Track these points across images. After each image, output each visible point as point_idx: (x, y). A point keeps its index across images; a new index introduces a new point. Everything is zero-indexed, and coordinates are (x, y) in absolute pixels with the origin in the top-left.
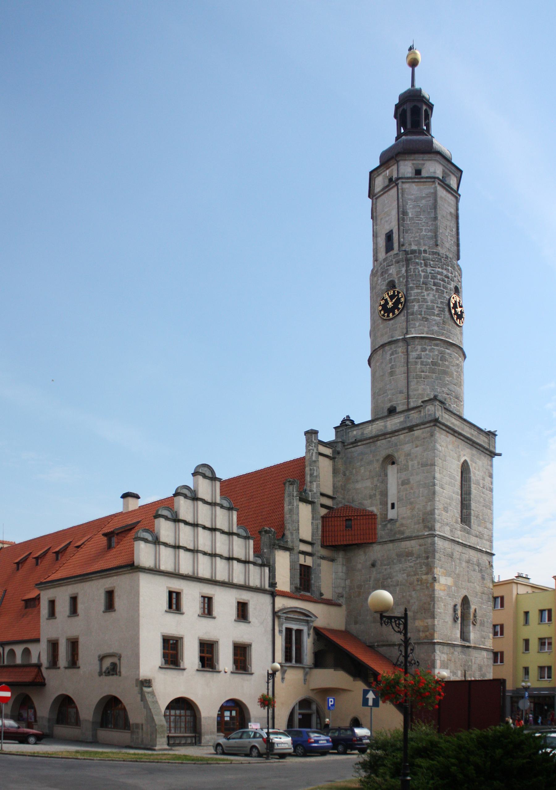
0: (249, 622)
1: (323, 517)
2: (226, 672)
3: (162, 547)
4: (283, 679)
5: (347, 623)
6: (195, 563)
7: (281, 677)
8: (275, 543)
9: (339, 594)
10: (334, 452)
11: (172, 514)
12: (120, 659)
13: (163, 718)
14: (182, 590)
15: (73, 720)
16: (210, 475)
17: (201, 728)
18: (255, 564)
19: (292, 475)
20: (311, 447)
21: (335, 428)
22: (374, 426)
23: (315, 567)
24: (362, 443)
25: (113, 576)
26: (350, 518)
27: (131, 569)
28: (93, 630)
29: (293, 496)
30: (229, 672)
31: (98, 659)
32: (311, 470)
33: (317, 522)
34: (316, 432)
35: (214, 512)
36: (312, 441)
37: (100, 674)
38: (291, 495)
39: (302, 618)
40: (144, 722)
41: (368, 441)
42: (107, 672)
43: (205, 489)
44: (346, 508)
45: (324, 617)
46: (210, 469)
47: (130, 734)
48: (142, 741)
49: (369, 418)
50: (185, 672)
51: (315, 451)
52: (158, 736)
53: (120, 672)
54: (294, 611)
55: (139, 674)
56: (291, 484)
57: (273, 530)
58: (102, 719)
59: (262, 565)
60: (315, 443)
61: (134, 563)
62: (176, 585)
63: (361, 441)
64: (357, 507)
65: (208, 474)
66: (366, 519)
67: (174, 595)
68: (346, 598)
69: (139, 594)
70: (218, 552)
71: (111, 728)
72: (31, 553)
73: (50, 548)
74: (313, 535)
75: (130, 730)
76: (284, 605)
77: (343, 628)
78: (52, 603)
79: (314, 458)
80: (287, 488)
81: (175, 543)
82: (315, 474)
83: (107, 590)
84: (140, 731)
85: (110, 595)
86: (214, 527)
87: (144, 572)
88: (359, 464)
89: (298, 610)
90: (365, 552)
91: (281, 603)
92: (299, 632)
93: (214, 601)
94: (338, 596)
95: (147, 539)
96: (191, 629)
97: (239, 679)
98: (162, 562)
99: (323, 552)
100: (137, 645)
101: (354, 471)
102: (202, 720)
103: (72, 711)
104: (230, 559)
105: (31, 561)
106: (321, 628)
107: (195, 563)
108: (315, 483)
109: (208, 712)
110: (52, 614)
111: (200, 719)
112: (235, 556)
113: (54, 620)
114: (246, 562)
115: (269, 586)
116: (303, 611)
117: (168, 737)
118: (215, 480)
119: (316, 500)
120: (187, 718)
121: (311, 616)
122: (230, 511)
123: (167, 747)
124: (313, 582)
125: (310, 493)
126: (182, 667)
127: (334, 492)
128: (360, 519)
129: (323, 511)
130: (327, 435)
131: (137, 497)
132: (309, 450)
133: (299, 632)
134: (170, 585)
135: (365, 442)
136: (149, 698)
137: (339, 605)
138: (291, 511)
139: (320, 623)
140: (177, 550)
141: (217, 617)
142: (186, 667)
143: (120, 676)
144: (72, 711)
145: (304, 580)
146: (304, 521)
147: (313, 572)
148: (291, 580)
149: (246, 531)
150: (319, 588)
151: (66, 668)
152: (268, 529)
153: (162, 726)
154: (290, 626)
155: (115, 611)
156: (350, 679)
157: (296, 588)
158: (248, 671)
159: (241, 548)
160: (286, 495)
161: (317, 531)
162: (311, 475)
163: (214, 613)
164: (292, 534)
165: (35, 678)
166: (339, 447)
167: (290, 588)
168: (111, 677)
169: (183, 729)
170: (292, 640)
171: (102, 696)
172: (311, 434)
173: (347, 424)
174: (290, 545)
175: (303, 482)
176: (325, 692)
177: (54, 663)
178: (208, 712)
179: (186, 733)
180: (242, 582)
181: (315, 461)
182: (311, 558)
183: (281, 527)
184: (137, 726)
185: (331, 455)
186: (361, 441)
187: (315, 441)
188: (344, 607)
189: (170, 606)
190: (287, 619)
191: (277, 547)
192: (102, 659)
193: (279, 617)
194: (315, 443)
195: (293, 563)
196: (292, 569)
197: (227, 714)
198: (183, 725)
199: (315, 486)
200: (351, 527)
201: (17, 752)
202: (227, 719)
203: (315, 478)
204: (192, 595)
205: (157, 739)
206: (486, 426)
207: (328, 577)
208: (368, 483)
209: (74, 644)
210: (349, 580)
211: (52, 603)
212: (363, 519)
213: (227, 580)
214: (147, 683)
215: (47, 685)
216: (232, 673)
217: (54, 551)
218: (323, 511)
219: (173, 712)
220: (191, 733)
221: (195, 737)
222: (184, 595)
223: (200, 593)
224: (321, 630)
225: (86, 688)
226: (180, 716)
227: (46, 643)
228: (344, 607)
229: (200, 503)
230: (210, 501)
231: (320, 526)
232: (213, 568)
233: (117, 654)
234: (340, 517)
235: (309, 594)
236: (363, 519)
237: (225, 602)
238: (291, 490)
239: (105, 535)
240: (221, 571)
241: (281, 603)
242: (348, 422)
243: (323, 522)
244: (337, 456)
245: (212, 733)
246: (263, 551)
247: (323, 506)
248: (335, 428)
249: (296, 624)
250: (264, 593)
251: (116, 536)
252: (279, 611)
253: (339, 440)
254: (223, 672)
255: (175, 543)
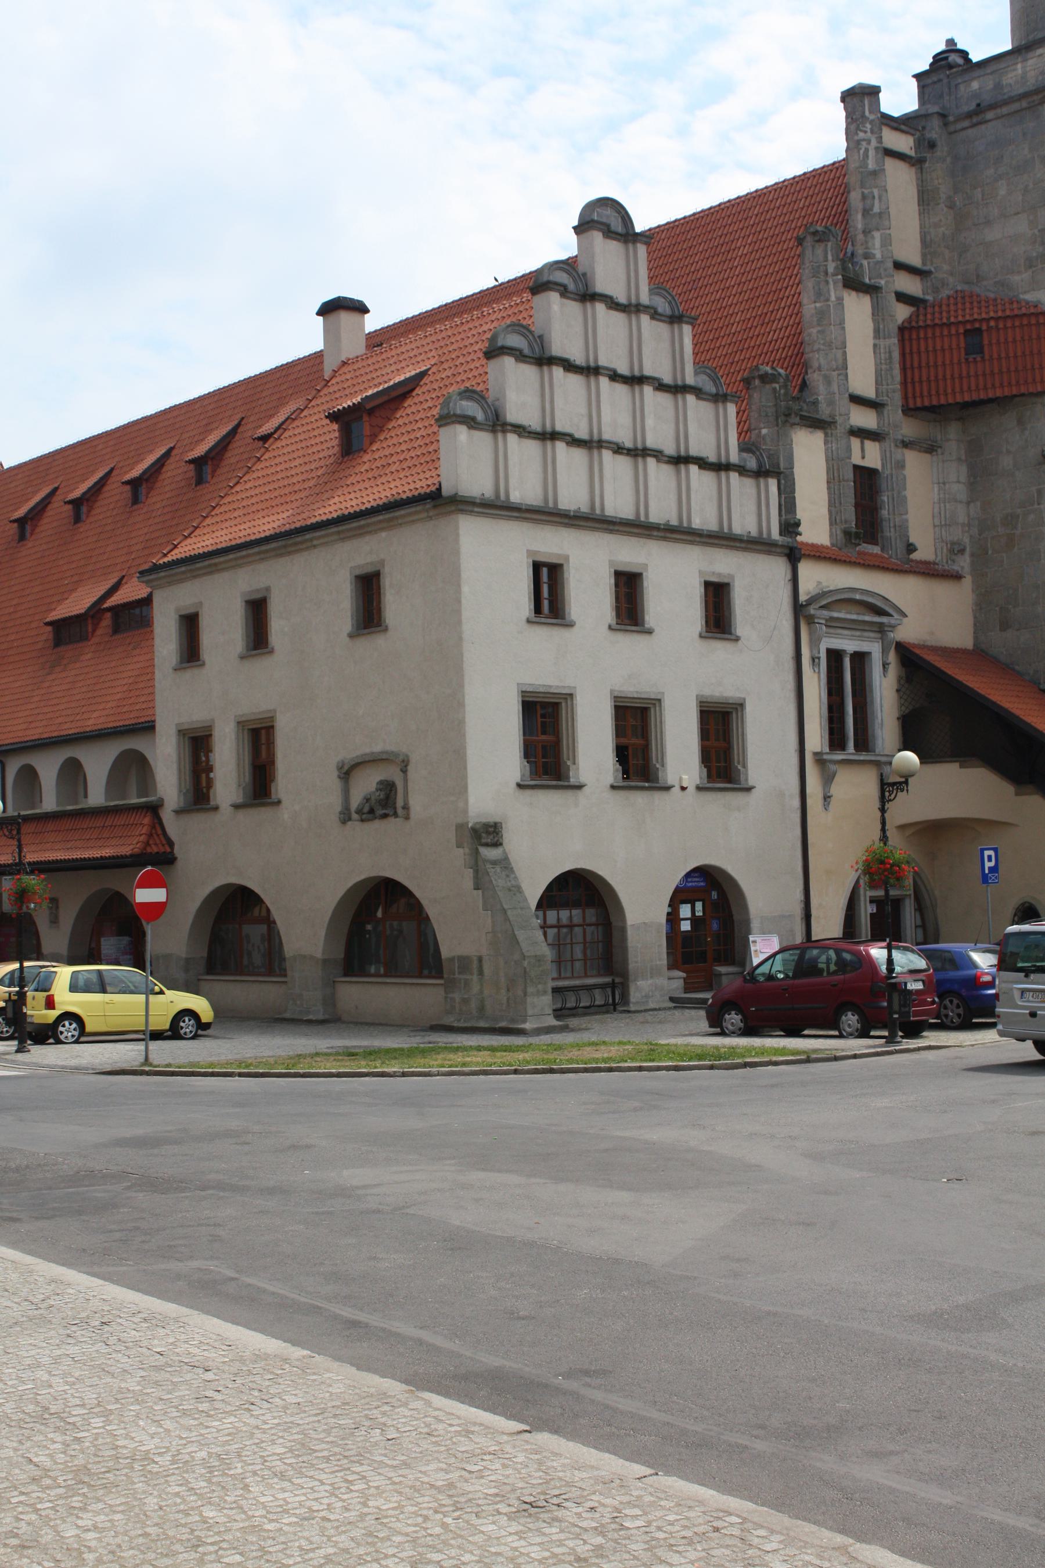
0: (737, 639)
1: (902, 329)
2: (683, 789)
3: (512, 438)
4: (827, 798)
5: (979, 627)
6: (594, 477)
7: (821, 796)
8: (788, 408)
9: (953, 543)
10: (918, 144)
11: (530, 345)
12: (404, 771)
13: (539, 934)
14: (567, 558)
15: (258, 959)
16: (620, 229)
17: (625, 961)
18: (742, 470)
19: (805, 216)
20: (861, 135)
21: (918, 77)
22: (1030, 62)
23: (888, 472)
24: (998, 111)
25: (376, 531)
26: (977, 325)
27: (435, 507)
28: (319, 692)
29: (826, 273)
30: (691, 789)
31: (336, 773)
32: (864, 197)
33: (888, 342)
34: (873, 92)
35: (634, 328)
36: (863, 116)
37: (345, 817)
38: (818, 272)
39: (867, 618)
40: (484, 952)
41: (1016, 106)
42: (366, 809)
43: (612, 270)
44: (961, 298)
45: (933, 614)
46: (619, 213)
47: (441, 991)
48: (482, 1009)
49: (1008, 47)
50: (581, 795)
51: (874, 143)
52: (530, 990)
53: (406, 807)
54: (848, 600)
55: (465, 811)
56: (819, 241)
57: (782, 371)
58: (211, 952)
59: (760, 473)
60: (871, 122)
61: (439, 489)
62: (553, 542)
63: (992, 107)
64: (992, 296)
65: (617, 226)
66: (1022, 326)
67: (545, 570)
68: (972, 555)
69: (459, 575)
70: (650, 443)
71: (377, 975)
72: (56, 490)
73: (112, 470)
74: (878, 383)
75: (441, 977)
76: (819, 583)
77: (968, 643)
78: (190, 624)
79: (871, 165)
80: (808, 253)
81: (544, 425)
82: (876, 209)
83: (358, 572)
84: (475, 977)
85: (369, 587)
86: (637, 373)
87: (471, 513)
88: (990, 172)
89: (858, 597)
90: (1020, 422)
91: (814, 577)
92: (860, 659)
93: (645, 584)
94: (951, 551)
95: (473, 419)
96: (591, 667)
97: (720, 804)
98: (513, 482)
99: (908, 429)
100: (459, 726)
101: (978, 193)
102: (630, 932)
103: (255, 932)
104: (680, 460)
105: (59, 510)
106: (915, 646)
107: (594, 477)
108: (877, 235)
109: (645, 909)
110: (191, 652)
111: (623, 930)
112: (694, 452)
113: (196, 671)
114: (720, 467)
115: (781, 534)
116: (870, 600)
117: (556, 990)
118: (634, 242)
119: (883, 282)
120: (589, 930)
121: (891, 611)
122: (676, 326)
123: (552, 1022)
124: (884, 513)
125: (865, 263)
126: (573, 781)
127: (924, 256)
128: (1005, 328)
129: (902, 312)
130: (900, 99)
131: (361, 309)
132: (858, 142)
133: (860, 659)
134: (535, 547)
135: (1005, 110)
136: (499, 881)
137: (957, 577)
138: (822, 315)
139: (908, 631)
140: (549, 444)
141: (657, 630)
142: (583, 778)
143: (407, 818)
144: (255, 932)
145: (866, 508)
146: (858, 346)
147: (884, 486)
148: (830, 512)
149: (715, 380)
150: (903, 529)
151: (237, 807)
152: (768, 369)
153: (539, 959)
154: (837, 643)
155: (386, 629)
156: (1009, 789)
157: (847, 533)
158: (738, 782)
159: (707, 428)
160: (806, 272)
161: (891, 369)
162: (866, 212)
163: (647, 618)
164: (828, 381)
165: (147, 844)
166: (934, 130)
167: (831, 536)
168: (377, 824)
169: (578, 965)
170: (845, 677)
171: (350, 884)
172: (860, 99)
173: (948, 67)
174: (824, 411)
175: (846, 237)
176: (933, 832)
177: (199, 795)
178: (645, 909)
179: (586, 976)
180: (712, 526)
181: (874, 173)
182: (877, 444)
183: (798, 362)
184: (464, 963)
185: (912, 153)
186: (992, 107)
187: (872, 117)
188: (967, 582)
189: (538, 609)
190: (832, 624)
191: (797, 420)
192: (347, 773)
193: (811, 620)
194: (871, 122)
195: (834, 463)
196: (833, 480)
197: (685, 911)
198: (578, 953)
199: (877, 243)
200: (982, 352)
201: (192, 1064)
202: (686, 926)
203: (876, 219)
204: (590, 570)
205: (529, 1000)
206: (838, 114)
207: (924, 498)
208: (1021, 226)
209: (259, 737)
210: (978, 504)
211: (190, 624)
212: (1013, 327)
213: (674, 522)
214: (488, 834)
215: (179, 864)
216: (699, 788)
217: (128, 477)
218: (902, 312)
219: (552, 916)
220: (599, 975)
221: (613, 986)
222: (572, 571)
223: (611, 563)
224: (917, 651)
225: (302, 864)
226: (571, 926)
227: (174, 739)
228: (967, 582)
229: (600, 307)
230: (622, 300)
231: (896, 355)
232: (640, 489)
233: (396, 755)
234: (949, 325)
235: (876, 550)
236: (1022, 326)
237: (675, 583)
238: (821, 258)
239: (334, 417)
240: (662, 494)
241: (814, 577)
242: (953, 58)
243: (902, 341)
244: (928, 155)
245: (654, 972)
246: (759, 435)
247: (902, 297)
248: (918, 77)
249: (852, 638)
250: (769, 553)
251: (366, 418)
252: (810, 602)
253: (931, 111)
254: (677, 789)
255: (544, 425)
